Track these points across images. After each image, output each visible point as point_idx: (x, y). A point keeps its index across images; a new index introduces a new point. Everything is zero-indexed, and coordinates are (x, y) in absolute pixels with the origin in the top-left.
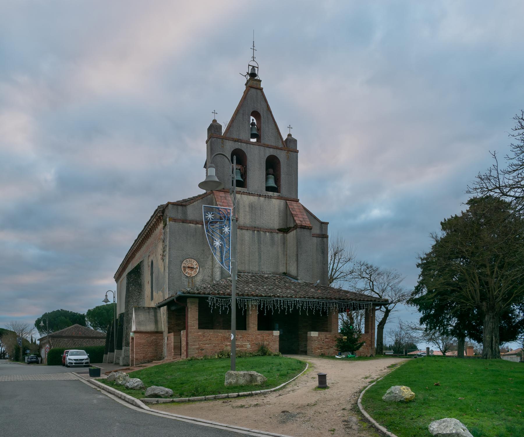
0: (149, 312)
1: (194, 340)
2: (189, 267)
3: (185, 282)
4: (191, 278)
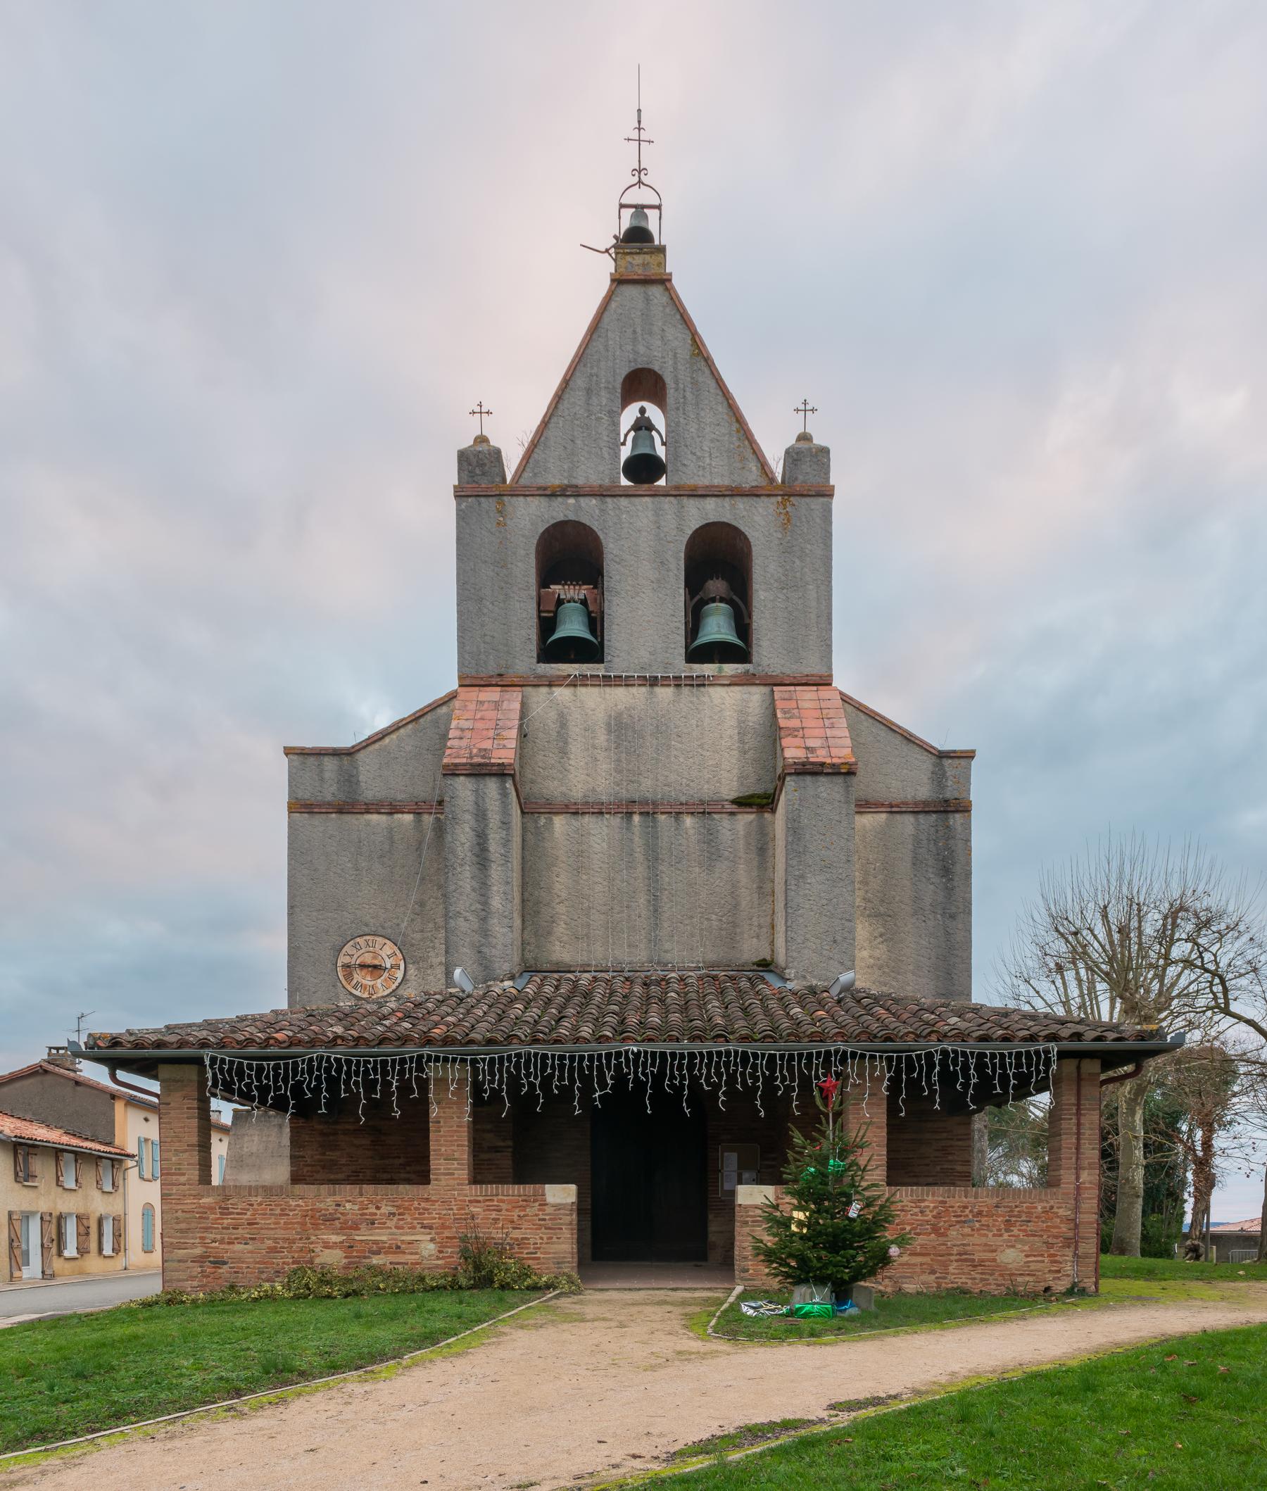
1: (183, 1226)
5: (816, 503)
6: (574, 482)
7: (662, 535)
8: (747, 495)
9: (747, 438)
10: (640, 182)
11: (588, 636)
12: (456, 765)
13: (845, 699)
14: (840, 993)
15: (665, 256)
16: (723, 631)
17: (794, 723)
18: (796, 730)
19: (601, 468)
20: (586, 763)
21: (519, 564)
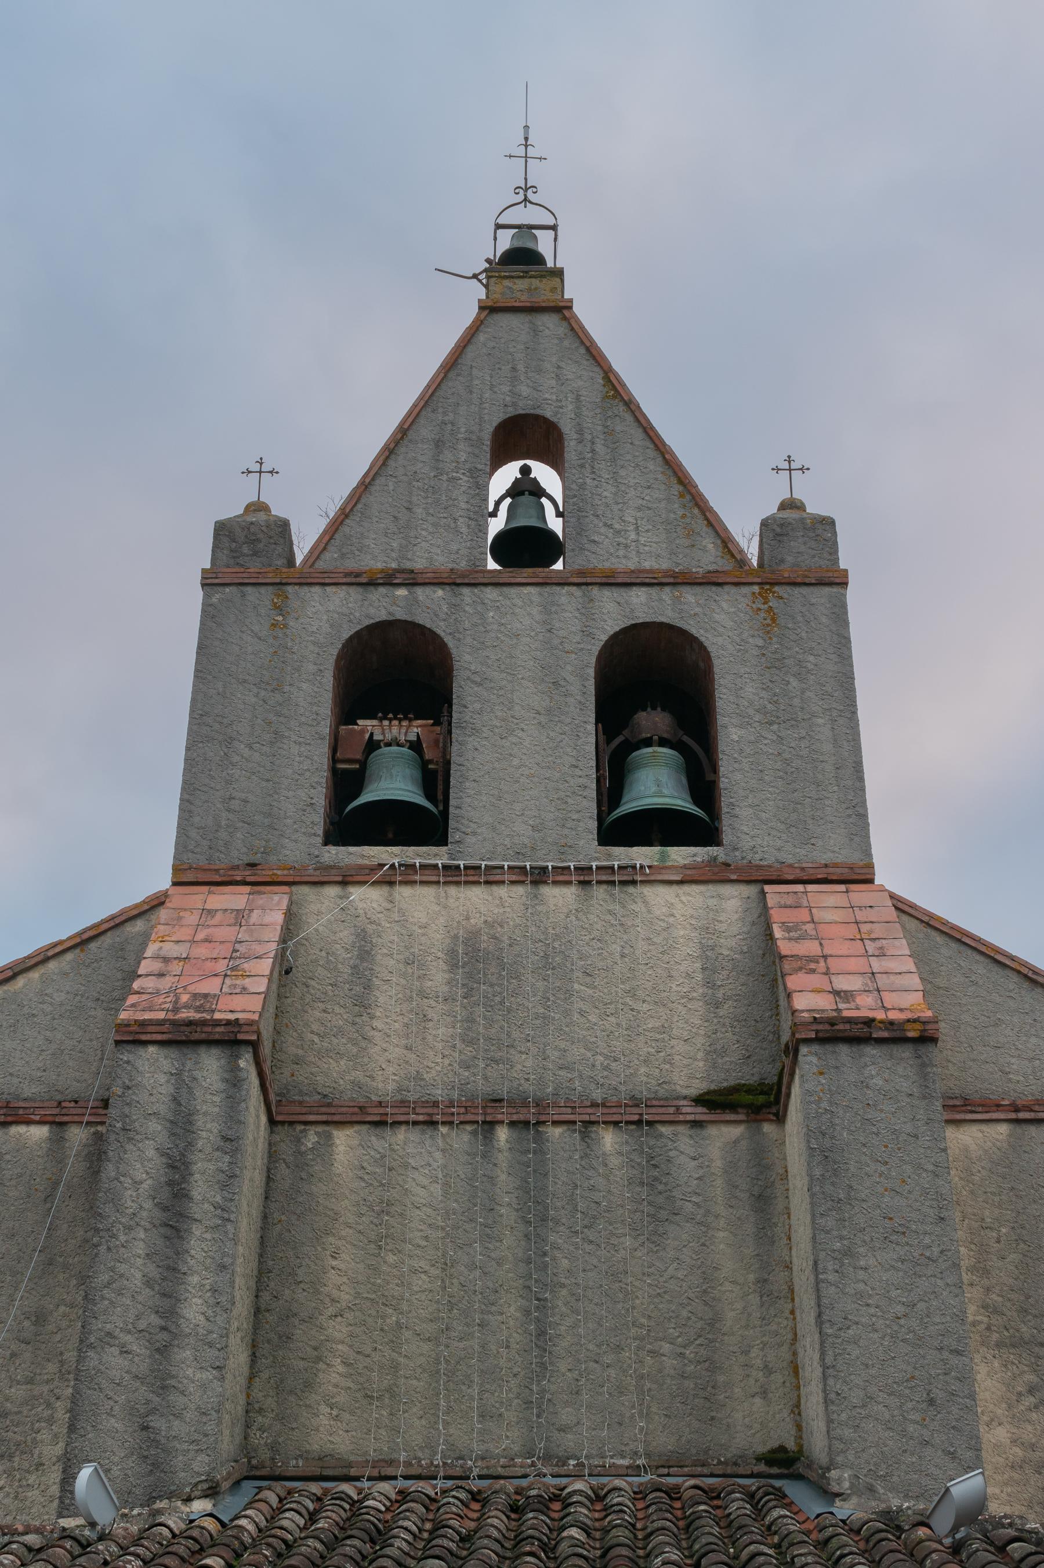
5: (820, 596)
6: (408, 565)
7: (556, 642)
8: (700, 584)
9: (697, 505)
10: (526, 199)
11: (421, 800)
12: (143, 1024)
13: (903, 907)
14: (955, 1529)
15: (562, 281)
16: (666, 792)
17: (810, 948)
18: (814, 959)
19: (454, 547)
20: (406, 1025)
21: (304, 686)
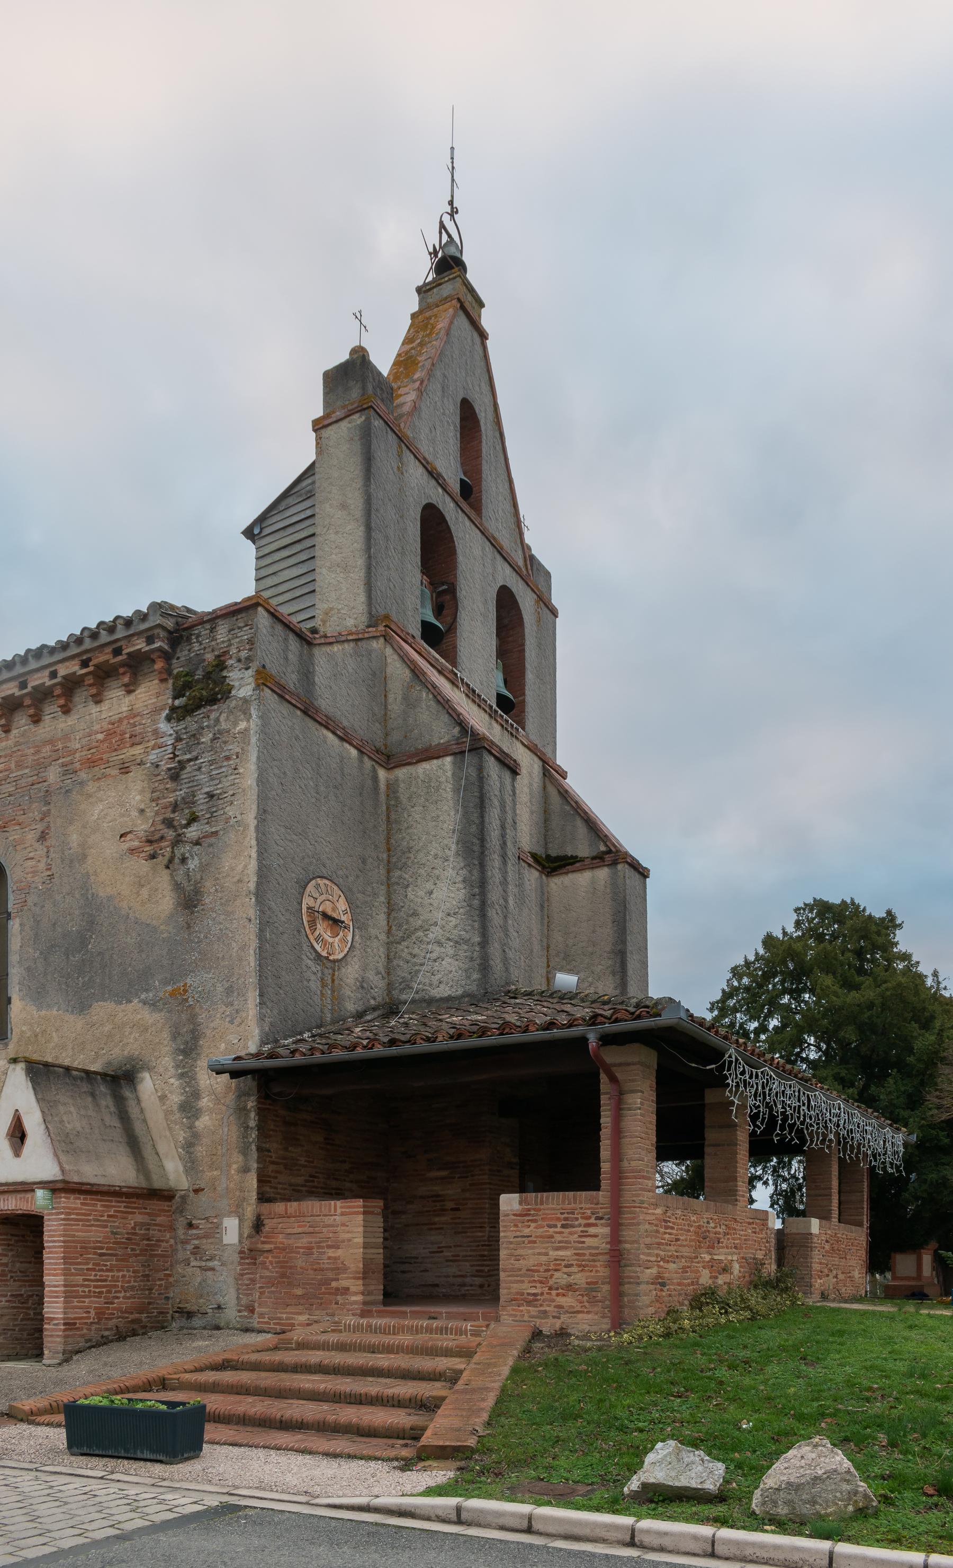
0: (93, 1095)
2: (325, 916)
3: (313, 978)
4: (329, 965)
